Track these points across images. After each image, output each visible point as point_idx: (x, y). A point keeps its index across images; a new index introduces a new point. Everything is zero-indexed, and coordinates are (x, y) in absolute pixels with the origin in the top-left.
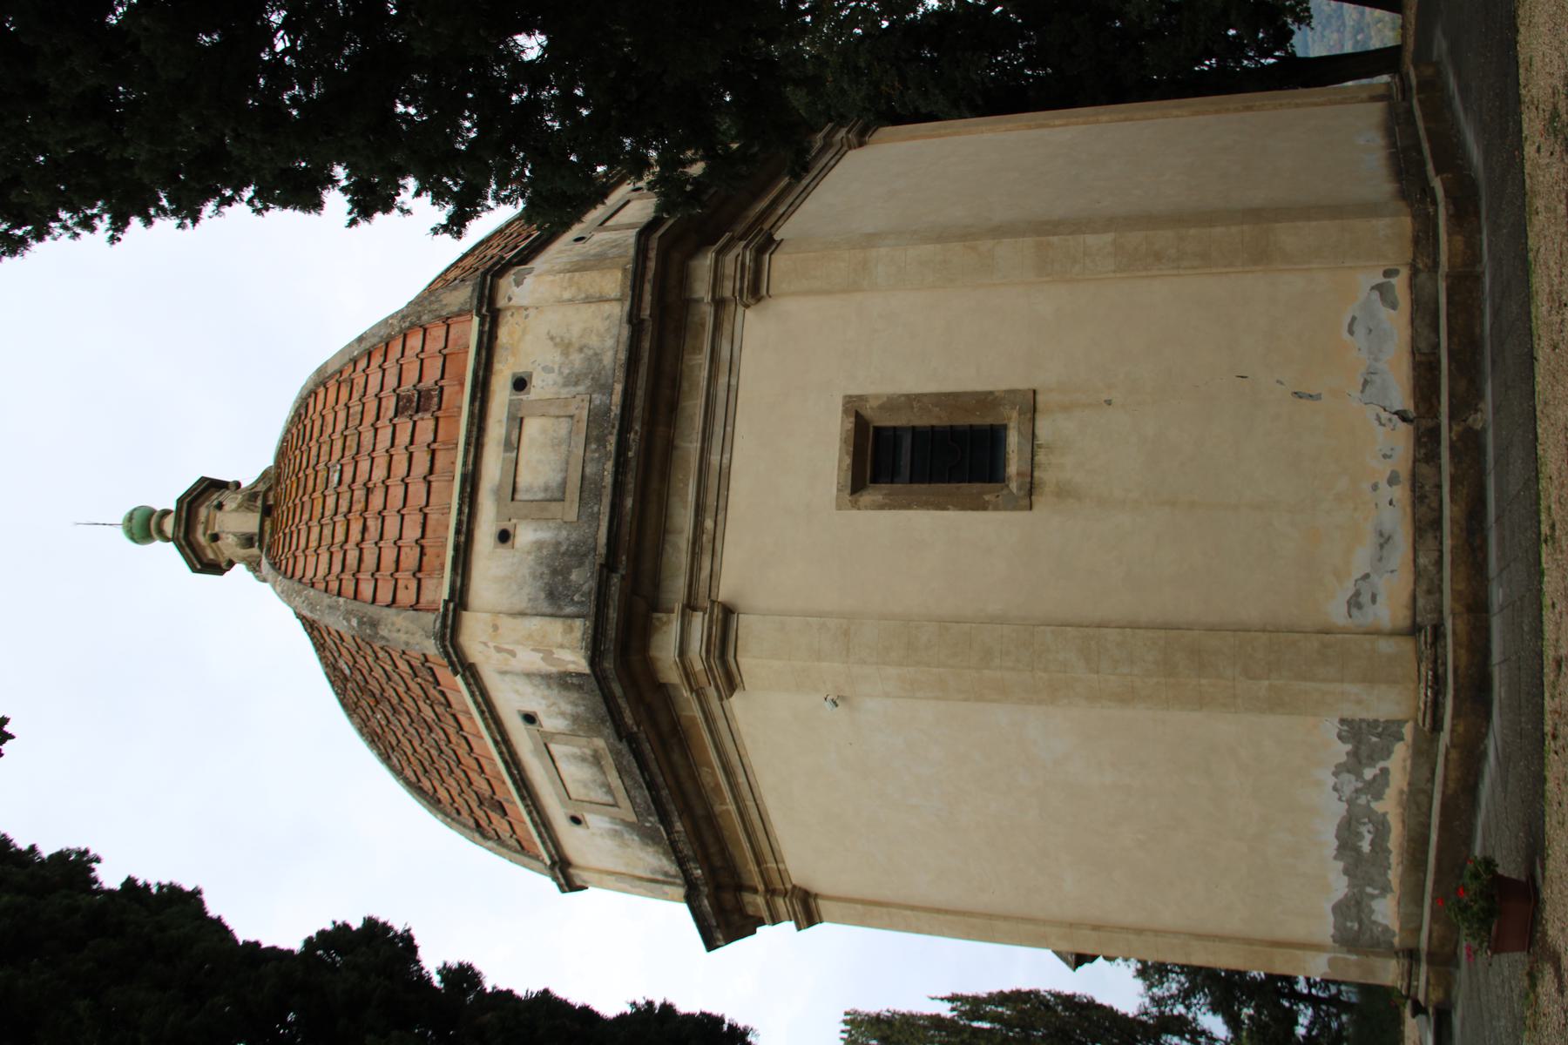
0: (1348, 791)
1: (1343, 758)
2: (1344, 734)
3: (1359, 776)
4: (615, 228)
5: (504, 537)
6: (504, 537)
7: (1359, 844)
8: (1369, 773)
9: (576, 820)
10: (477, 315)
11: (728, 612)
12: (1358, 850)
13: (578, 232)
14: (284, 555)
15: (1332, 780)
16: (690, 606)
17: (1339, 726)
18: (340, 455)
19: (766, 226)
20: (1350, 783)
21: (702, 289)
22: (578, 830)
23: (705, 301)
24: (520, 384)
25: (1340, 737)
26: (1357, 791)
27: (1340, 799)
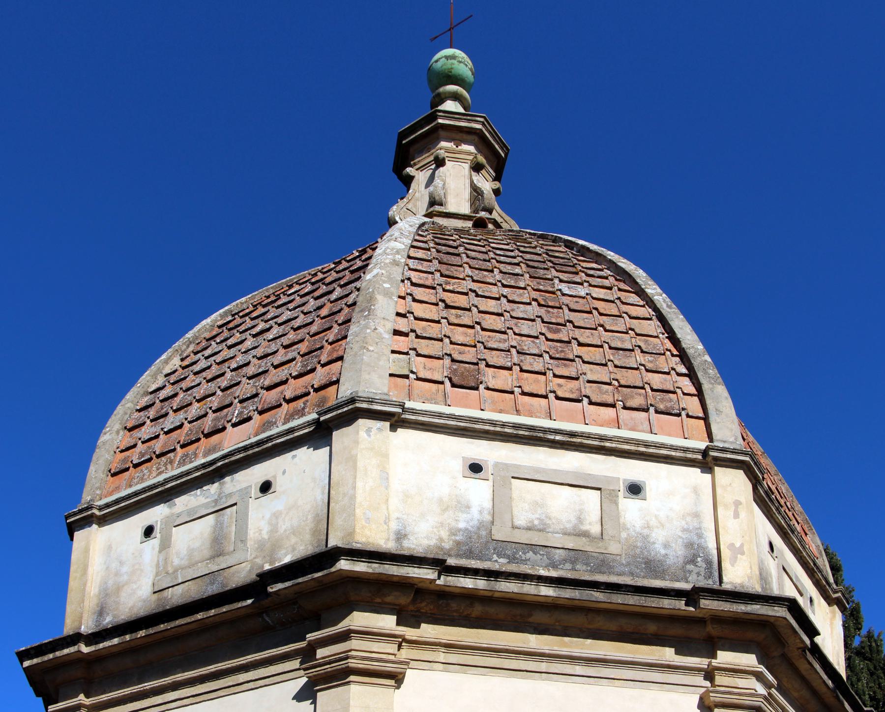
24: (635, 489)
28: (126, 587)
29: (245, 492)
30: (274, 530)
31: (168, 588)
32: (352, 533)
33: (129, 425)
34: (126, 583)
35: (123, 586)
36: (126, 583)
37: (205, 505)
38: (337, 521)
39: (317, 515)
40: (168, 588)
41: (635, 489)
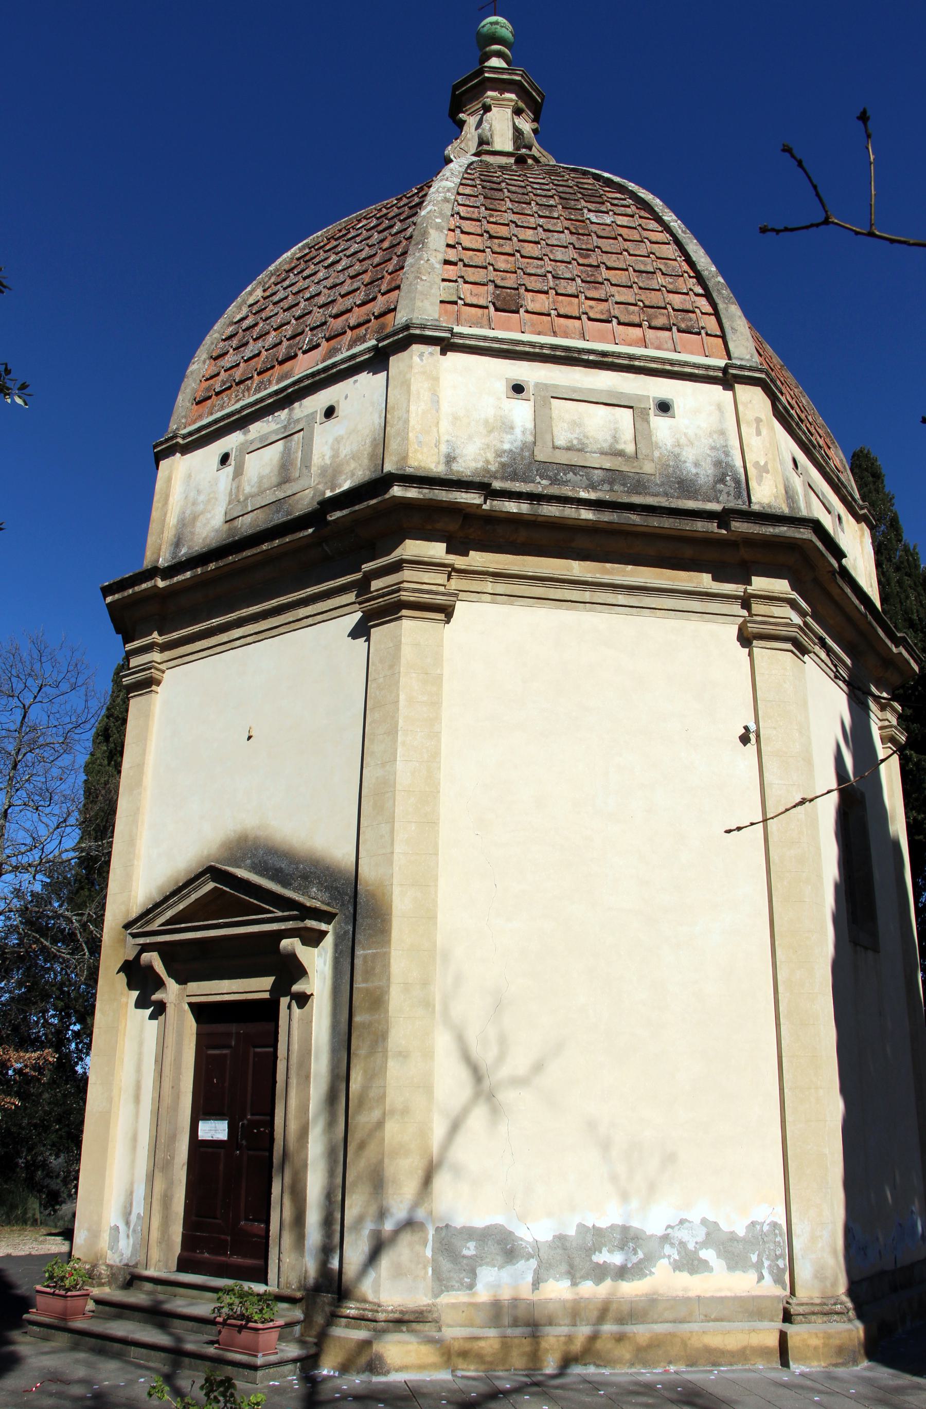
0: (681, 1234)
1: (725, 1227)
2: (758, 1227)
3: (705, 1244)
4: (806, 496)
5: (518, 389)
6: (518, 389)
7: (604, 1250)
8: (708, 1254)
9: (225, 459)
10: (726, 364)
11: (447, 612)
12: (597, 1248)
13: (802, 462)
14: (528, 183)
15: (695, 1217)
16: (451, 571)
17: (768, 1222)
18: (654, 239)
19: (817, 649)
20: (692, 1237)
21: (760, 584)
22: (216, 459)
23: (749, 587)
24: (664, 407)
25: (753, 1224)
26: (682, 1244)
27: (669, 1227)
28: (201, 517)
29: (311, 417)
30: (335, 455)
31: (239, 517)
32: (405, 458)
33: (214, 355)
34: (202, 513)
35: (199, 516)
36: (202, 513)
37: (275, 432)
38: (393, 445)
39: (375, 439)
40: (239, 517)
41: (664, 407)
